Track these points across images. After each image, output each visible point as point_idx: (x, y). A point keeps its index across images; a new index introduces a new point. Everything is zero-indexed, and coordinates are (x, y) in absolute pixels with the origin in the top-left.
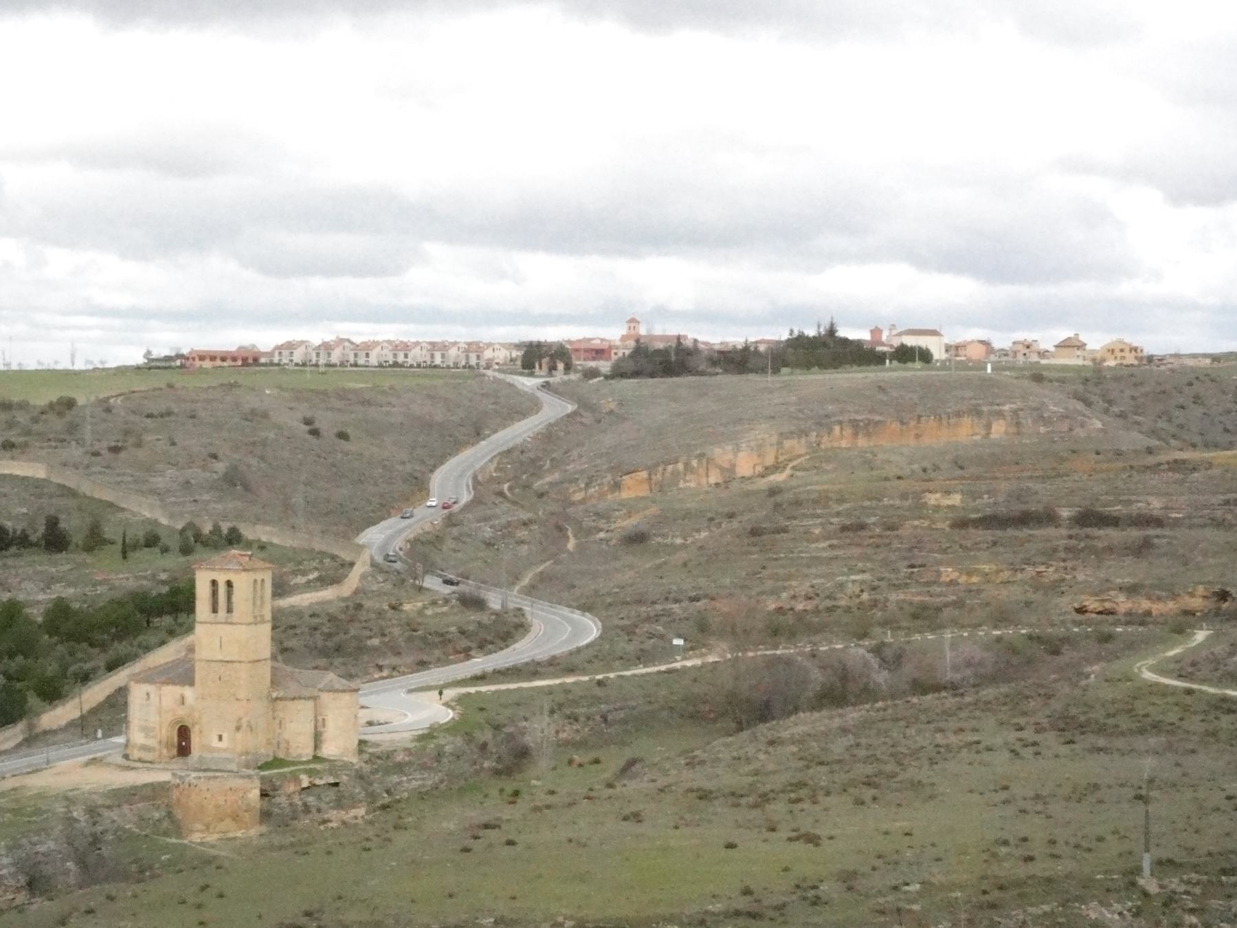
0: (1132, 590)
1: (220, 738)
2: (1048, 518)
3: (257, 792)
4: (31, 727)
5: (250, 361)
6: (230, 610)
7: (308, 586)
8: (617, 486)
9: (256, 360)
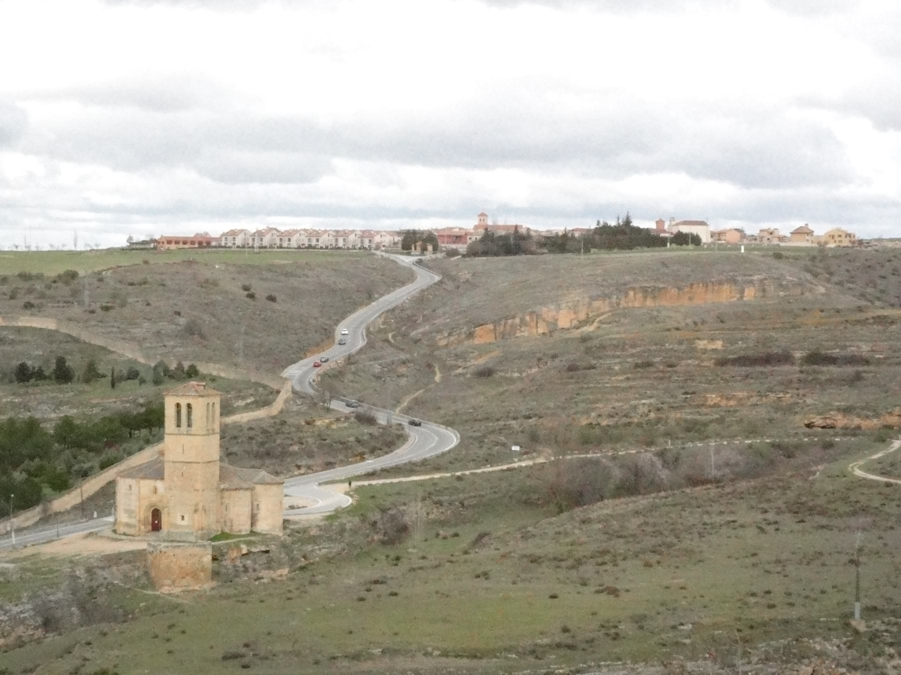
0: (847, 411)
1: (183, 517)
2: (785, 358)
3: (210, 557)
4: (45, 510)
5: (205, 244)
6: (189, 425)
7: (247, 408)
8: (470, 335)
9: (208, 243)
